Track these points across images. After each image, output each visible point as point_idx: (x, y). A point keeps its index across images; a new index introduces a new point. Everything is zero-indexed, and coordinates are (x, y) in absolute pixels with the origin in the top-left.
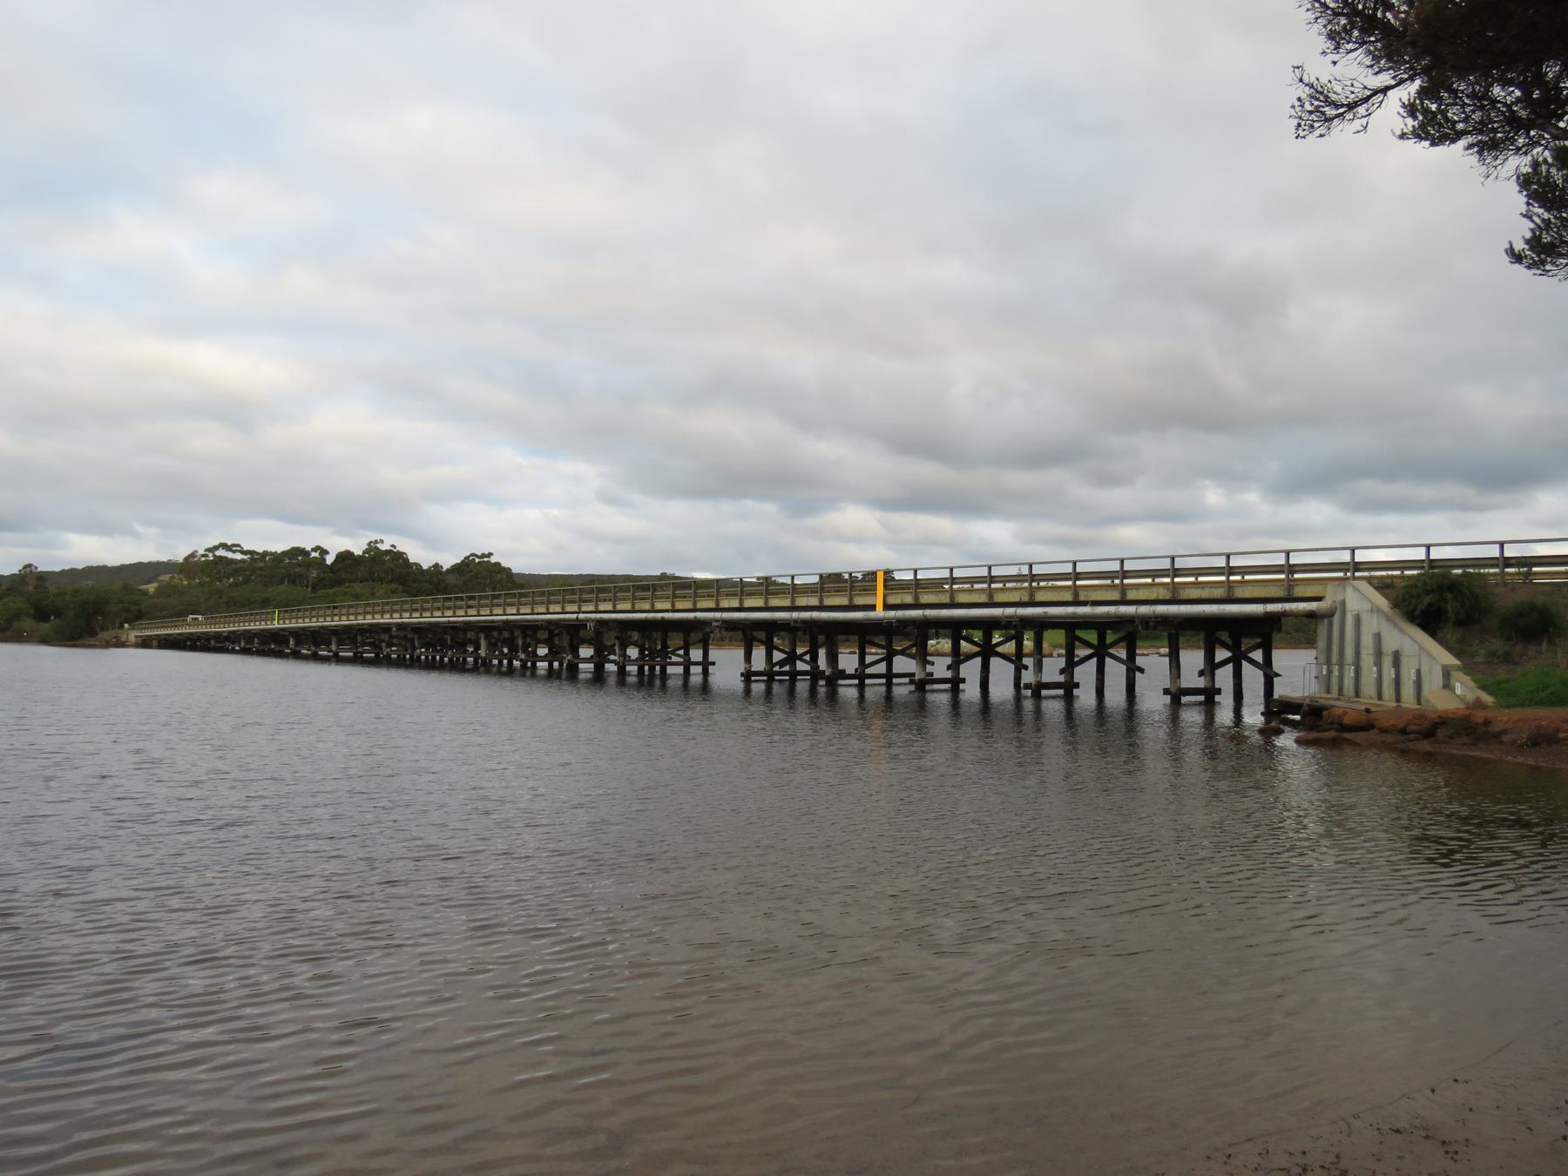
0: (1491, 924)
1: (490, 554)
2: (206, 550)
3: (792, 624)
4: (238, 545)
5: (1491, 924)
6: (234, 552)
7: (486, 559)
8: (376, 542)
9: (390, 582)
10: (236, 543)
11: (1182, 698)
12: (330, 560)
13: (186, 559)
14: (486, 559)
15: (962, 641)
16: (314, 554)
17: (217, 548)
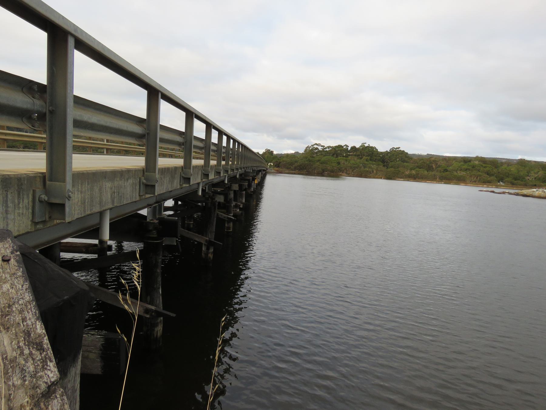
0: (479, 191)
1: (399, 148)
2: (311, 145)
3: (513, 169)
4: (320, 144)
5: (479, 191)
6: (319, 146)
7: (398, 149)
8: (364, 143)
9: (367, 156)
10: (319, 143)
11: (225, 163)
12: (349, 149)
13: (305, 151)
14: (398, 149)
15: (179, 202)
16: (344, 147)
17: (314, 145)
